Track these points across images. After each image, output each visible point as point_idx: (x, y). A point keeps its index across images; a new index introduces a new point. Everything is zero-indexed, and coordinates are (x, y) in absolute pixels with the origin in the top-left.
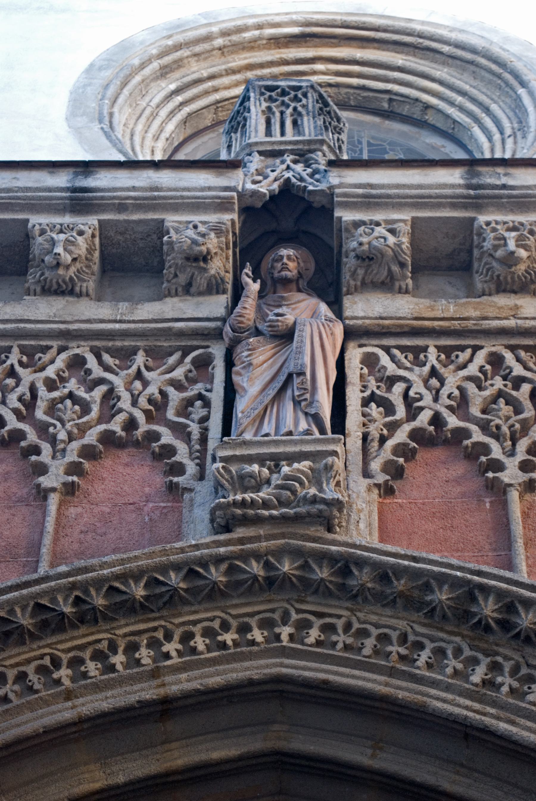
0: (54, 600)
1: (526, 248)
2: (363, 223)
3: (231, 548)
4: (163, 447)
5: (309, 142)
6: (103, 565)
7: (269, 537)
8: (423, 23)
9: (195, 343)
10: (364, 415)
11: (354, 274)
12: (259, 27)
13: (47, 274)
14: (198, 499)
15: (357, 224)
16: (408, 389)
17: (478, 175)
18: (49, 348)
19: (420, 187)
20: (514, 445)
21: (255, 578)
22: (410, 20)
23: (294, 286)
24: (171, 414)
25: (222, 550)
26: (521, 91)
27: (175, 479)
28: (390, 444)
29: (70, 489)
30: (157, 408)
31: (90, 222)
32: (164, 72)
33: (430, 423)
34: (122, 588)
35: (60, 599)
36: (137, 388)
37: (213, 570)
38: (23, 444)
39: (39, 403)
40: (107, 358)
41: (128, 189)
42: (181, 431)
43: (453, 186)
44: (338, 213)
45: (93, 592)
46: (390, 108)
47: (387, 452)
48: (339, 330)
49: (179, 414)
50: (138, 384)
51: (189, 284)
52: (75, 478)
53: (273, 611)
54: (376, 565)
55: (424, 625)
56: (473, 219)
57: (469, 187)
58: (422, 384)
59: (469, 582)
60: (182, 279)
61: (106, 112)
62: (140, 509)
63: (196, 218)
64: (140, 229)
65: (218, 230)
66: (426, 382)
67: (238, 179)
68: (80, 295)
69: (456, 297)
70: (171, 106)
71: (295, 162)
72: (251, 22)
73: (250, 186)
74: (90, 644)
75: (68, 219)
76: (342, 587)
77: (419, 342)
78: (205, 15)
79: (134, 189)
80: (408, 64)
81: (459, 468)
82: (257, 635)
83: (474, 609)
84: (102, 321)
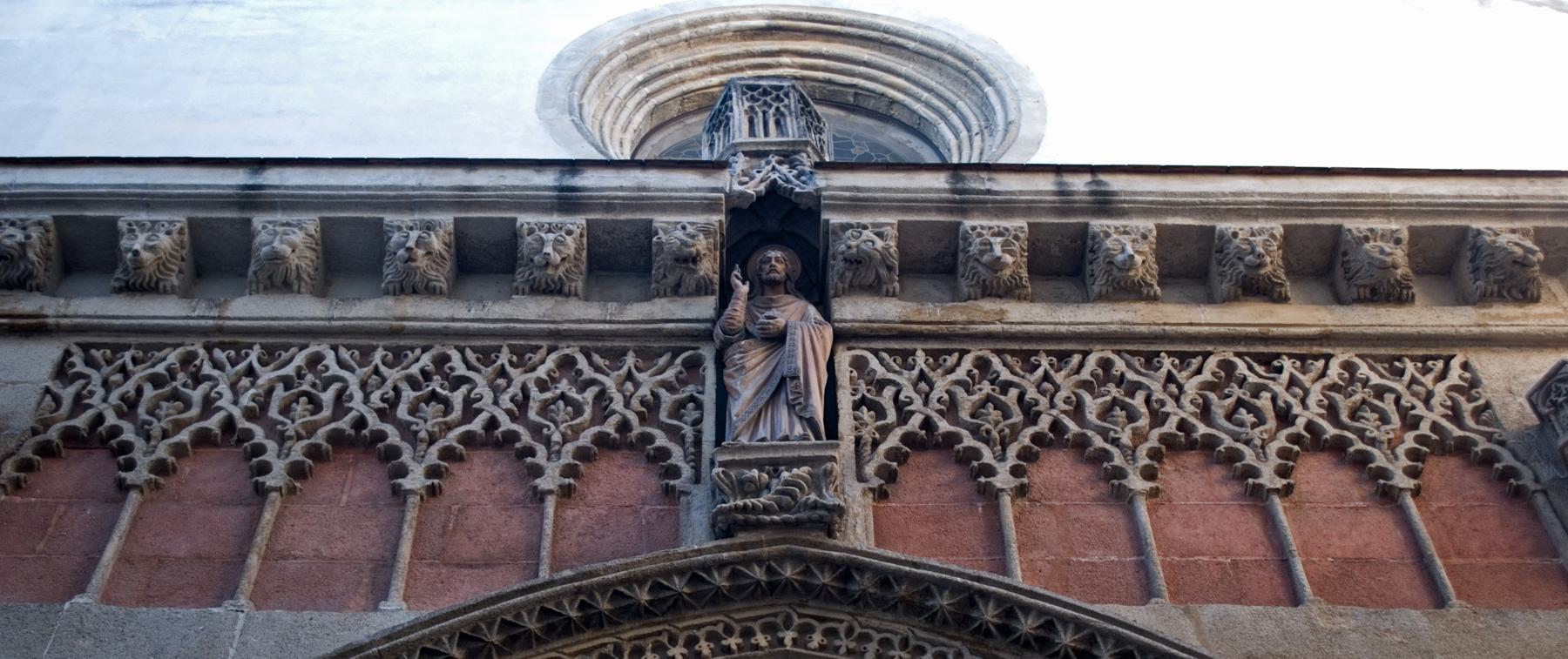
0: (560, 604)
1: (1011, 253)
2: (850, 226)
3: (733, 553)
4: (658, 449)
5: (794, 143)
6: (607, 570)
7: (769, 543)
8: (889, 18)
9: (685, 344)
10: (856, 419)
11: (842, 277)
12: (726, 19)
13: (536, 273)
14: (696, 502)
15: (845, 227)
16: (898, 393)
17: (963, 179)
18: (539, 348)
19: (906, 190)
20: (1004, 450)
21: (758, 583)
22: (876, 15)
23: (782, 288)
24: (663, 416)
25: (725, 555)
26: (988, 89)
27: (672, 482)
28: (883, 448)
29: (566, 492)
30: (650, 409)
31: (578, 221)
32: (631, 63)
33: (921, 427)
34: (627, 592)
35: (566, 603)
36: (632, 388)
37: (716, 575)
38: (518, 445)
39: (531, 403)
40: (596, 358)
41: (616, 189)
42: (674, 433)
43: (938, 190)
44: (825, 216)
45: (598, 597)
46: (856, 103)
47: (880, 457)
48: (828, 333)
49: (670, 416)
50: (629, 386)
51: (678, 285)
52: (571, 481)
53: (775, 615)
54: (877, 571)
55: (925, 630)
56: (959, 224)
57: (954, 191)
58: (911, 388)
59: (970, 588)
60: (671, 280)
61: (576, 104)
62: (636, 512)
63: (685, 219)
64: (628, 229)
65: (706, 231)
66: (915, 385)
67: (724, 180)
68: (568, 295)
69: (941, 301)
70: (638, 97)
71: (780, 163)
72: (717, 14)
73: (737, 187)
74: (595, 647)
75: (555, 219)
76: (843, 592)
77: (907, 345)
78: (672, 6)
79: (622, 188)
80: (873, 59)
81: (950, 473)
82: (761, 639)
83: (975, 614)
84: (591, 321)
